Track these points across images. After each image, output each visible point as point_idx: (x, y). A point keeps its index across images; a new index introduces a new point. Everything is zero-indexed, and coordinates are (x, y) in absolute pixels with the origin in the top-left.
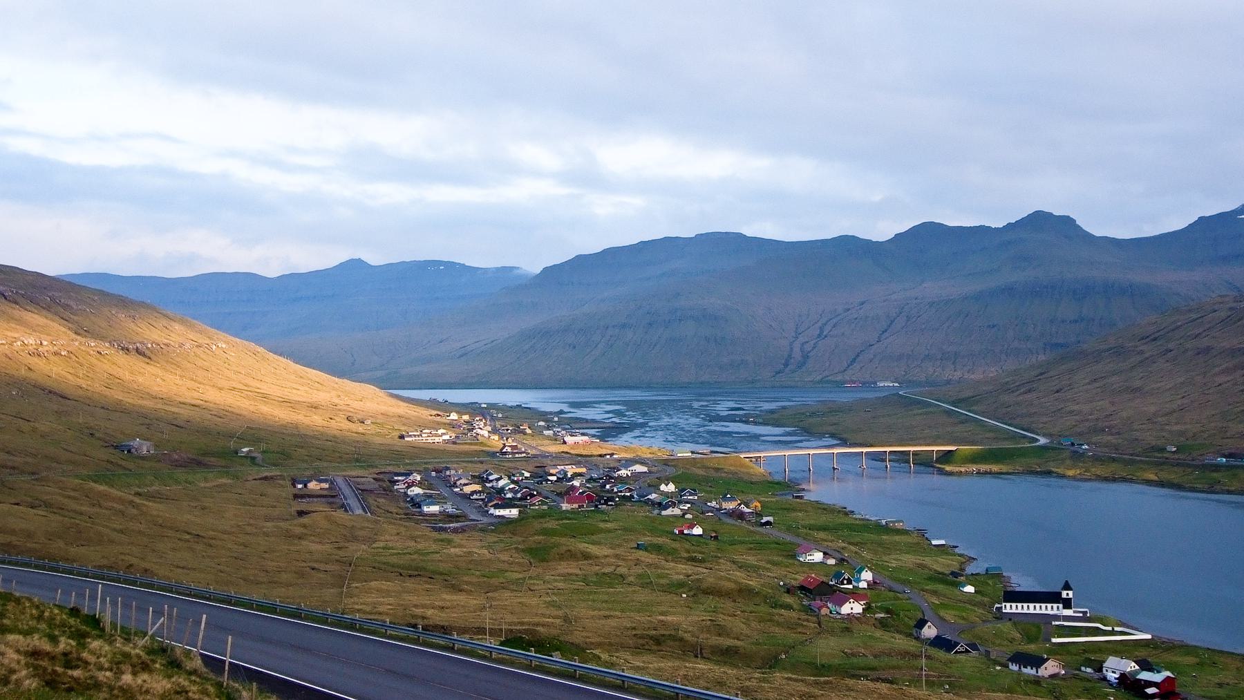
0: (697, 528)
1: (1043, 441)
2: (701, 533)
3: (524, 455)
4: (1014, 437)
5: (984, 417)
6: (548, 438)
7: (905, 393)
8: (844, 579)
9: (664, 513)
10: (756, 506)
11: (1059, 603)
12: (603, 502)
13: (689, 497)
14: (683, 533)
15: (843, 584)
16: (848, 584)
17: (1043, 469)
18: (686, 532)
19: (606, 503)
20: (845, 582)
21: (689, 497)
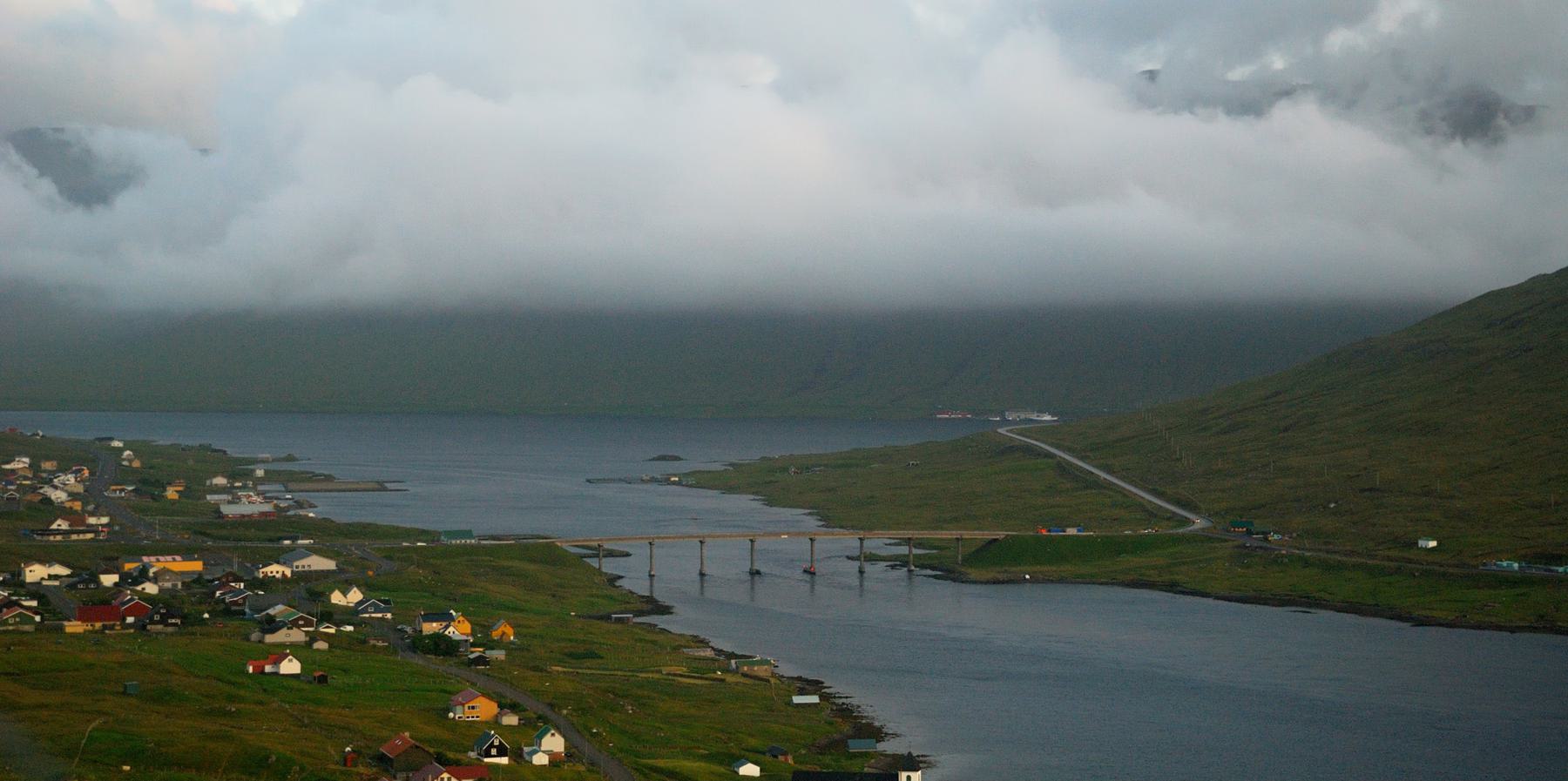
0: (290, 661)
1: (1199, 523)
2: (299, 672)
3: (90, 536)
4: (1152, 515)
5: (1131, 483)
6: (674, 483)
7: (1011, 431)
8: (492, 746)
9: (269, 638)
10: (504, 633)
11: (549, 730)
12: (157, 617)
13: (373, 615)
14: (263, 672)
15: (489, 755)
16: (500, 754)
17: (1166, 578)
18: (268, 669)
19: (163, 621)
20: (494, 751)
21: (373, 615)
